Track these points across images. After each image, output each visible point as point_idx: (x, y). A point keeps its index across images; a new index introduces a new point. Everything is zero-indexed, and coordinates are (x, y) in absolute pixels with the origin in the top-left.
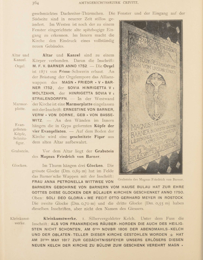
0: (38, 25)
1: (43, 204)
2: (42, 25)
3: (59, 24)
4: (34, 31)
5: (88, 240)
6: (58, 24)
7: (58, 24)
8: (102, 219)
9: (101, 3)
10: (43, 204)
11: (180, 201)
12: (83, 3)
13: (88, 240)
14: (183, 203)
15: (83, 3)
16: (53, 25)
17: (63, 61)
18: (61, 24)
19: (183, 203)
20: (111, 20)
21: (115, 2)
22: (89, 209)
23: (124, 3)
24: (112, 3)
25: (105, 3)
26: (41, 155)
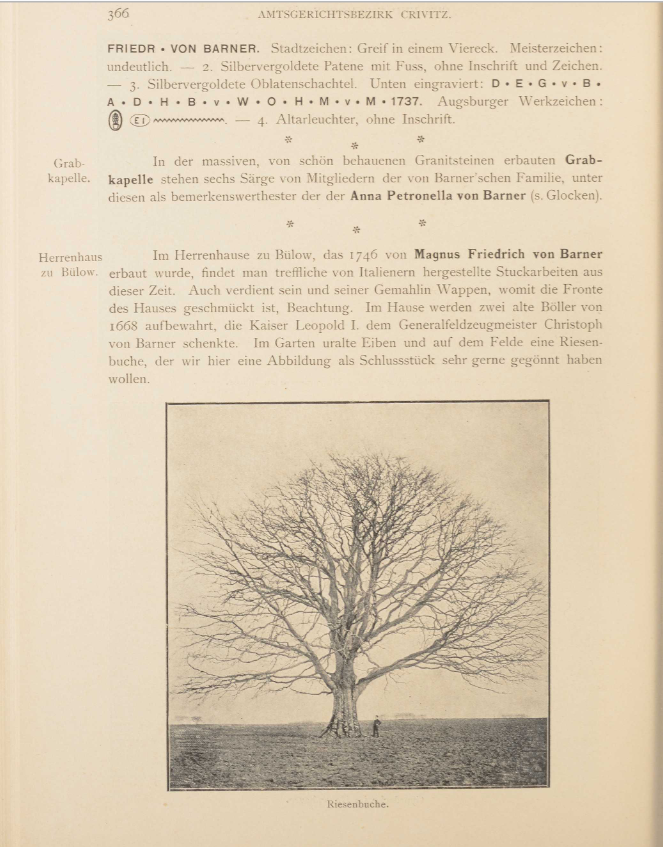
0: (125, 68)
1: (485, 308)
2: (473, 85)
3: (529, 98)
4: (496, 345)
5: (137, 50)
6: (524, 98)
7: (524, 98)
8: (189, 87)
9: (332, 14)
10: (485, 308)
11: (589, 352)
12: (271, 14)
13: (137, 47)
14: (599, 360)
15: (271, 14)
16: (166, 257)
17: (125, 68)
18: (533, 99)
19: (599, 360)
20: (190, 311)
21: (377, 14)
22: (158, 68)
23: (405, 14)
24: (365, 14)
25: (343, 15)
26: (417, 250)
